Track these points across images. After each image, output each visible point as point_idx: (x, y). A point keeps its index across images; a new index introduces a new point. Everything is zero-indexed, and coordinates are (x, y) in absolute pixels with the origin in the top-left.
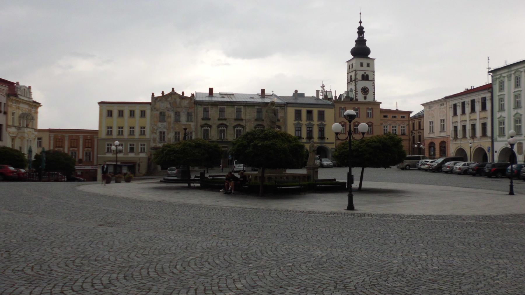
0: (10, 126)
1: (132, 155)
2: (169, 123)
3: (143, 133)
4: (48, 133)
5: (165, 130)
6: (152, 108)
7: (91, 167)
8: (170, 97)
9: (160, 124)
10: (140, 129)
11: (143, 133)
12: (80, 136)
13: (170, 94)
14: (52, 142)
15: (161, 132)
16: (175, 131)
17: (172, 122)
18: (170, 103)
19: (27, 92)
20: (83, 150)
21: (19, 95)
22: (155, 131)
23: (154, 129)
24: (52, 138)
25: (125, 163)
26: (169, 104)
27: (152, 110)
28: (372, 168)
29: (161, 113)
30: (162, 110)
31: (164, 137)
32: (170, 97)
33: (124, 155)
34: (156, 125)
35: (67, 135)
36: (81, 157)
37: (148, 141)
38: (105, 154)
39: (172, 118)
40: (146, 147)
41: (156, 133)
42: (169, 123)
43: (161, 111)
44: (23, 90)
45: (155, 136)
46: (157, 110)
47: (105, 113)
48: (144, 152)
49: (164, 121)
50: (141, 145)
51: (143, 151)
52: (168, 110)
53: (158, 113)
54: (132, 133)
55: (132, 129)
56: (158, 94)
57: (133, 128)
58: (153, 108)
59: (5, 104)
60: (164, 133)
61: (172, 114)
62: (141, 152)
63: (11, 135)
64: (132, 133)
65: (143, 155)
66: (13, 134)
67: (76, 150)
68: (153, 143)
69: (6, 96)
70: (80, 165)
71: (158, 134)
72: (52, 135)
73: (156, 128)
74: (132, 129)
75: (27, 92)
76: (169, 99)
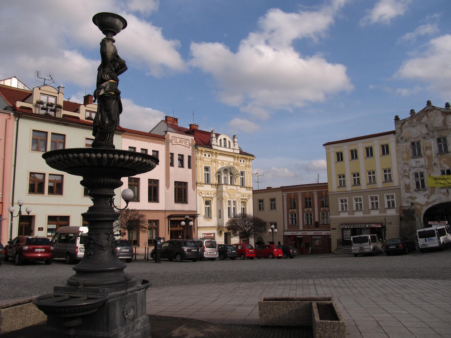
0: (201, 184)
1: (375, 213)
2: (429, 158)
3: (388, 178)
4: (280, 193)
5: (422, 170)
6: (397, 140)
7: (308, 234)
8: (426, 117)
9: (413, 162)
10: (384, 174)
11: (388, 178)
12: (313, 193)
13: (425, 111)
14: (285, 203)
15: (416, 175)
16: (441, 169)
17: (434, 155)
18: (426, 126)
19: (229, 142)
20: (319, 211)
21: (214, 145)
22: (406, 174)
23: (405, 171)
24: (285, 198)
25: (189, 237)
26: (425, 126)
27: (397, 142)
28: (299, 211)
29: (413, 144)
30: (415, 138)
31: (423, 181)
32: (426, 117)
33: (349, 214)
34: (407, 164)
35: (299, 193)
36: (317, 220)
37: (398, 189)
38: (339, 213)
39: (433, 149)
40: (395, 200)
41: (408, 177)
42: (429, 158)
43: (413, 140)
44: (223, 141)
45: (407, 181)
46: (406, 141)
47: (334, 157)
48: (377, 208)
49: (420, 155)
50: (388, 197)
51: (391, 205)
52: (424, 138)
53: (409, 144)
54: (372, 179)
55: (371, 173)
56: (404, 115)
57: (374, 173)
58: (399, 138)
59: (189, 157)
60: (422, 174)
61: (433, 143)
62: (389, 207)
63: (203, 195)
64: (372, 179)
65: (392, 212)
66: (208, 194)
67: (295, 211)
68: (406, 192)
69: (191, 147)
70: (316, 229)
71: (412, 177)
72: (285, 194)
73: (407, 169)
74: (371, 173)
75: (229, 142)
76: (424, 119)
